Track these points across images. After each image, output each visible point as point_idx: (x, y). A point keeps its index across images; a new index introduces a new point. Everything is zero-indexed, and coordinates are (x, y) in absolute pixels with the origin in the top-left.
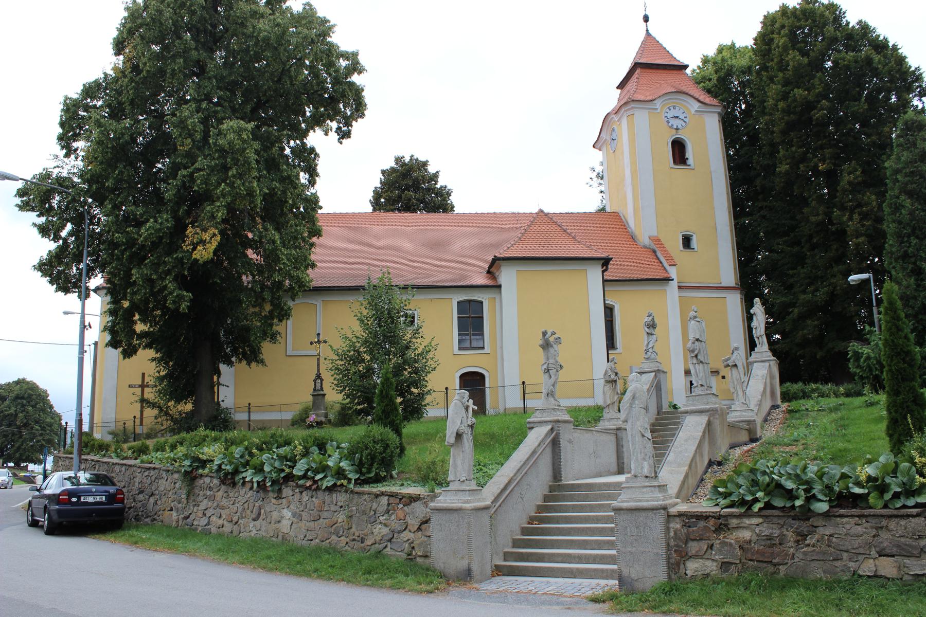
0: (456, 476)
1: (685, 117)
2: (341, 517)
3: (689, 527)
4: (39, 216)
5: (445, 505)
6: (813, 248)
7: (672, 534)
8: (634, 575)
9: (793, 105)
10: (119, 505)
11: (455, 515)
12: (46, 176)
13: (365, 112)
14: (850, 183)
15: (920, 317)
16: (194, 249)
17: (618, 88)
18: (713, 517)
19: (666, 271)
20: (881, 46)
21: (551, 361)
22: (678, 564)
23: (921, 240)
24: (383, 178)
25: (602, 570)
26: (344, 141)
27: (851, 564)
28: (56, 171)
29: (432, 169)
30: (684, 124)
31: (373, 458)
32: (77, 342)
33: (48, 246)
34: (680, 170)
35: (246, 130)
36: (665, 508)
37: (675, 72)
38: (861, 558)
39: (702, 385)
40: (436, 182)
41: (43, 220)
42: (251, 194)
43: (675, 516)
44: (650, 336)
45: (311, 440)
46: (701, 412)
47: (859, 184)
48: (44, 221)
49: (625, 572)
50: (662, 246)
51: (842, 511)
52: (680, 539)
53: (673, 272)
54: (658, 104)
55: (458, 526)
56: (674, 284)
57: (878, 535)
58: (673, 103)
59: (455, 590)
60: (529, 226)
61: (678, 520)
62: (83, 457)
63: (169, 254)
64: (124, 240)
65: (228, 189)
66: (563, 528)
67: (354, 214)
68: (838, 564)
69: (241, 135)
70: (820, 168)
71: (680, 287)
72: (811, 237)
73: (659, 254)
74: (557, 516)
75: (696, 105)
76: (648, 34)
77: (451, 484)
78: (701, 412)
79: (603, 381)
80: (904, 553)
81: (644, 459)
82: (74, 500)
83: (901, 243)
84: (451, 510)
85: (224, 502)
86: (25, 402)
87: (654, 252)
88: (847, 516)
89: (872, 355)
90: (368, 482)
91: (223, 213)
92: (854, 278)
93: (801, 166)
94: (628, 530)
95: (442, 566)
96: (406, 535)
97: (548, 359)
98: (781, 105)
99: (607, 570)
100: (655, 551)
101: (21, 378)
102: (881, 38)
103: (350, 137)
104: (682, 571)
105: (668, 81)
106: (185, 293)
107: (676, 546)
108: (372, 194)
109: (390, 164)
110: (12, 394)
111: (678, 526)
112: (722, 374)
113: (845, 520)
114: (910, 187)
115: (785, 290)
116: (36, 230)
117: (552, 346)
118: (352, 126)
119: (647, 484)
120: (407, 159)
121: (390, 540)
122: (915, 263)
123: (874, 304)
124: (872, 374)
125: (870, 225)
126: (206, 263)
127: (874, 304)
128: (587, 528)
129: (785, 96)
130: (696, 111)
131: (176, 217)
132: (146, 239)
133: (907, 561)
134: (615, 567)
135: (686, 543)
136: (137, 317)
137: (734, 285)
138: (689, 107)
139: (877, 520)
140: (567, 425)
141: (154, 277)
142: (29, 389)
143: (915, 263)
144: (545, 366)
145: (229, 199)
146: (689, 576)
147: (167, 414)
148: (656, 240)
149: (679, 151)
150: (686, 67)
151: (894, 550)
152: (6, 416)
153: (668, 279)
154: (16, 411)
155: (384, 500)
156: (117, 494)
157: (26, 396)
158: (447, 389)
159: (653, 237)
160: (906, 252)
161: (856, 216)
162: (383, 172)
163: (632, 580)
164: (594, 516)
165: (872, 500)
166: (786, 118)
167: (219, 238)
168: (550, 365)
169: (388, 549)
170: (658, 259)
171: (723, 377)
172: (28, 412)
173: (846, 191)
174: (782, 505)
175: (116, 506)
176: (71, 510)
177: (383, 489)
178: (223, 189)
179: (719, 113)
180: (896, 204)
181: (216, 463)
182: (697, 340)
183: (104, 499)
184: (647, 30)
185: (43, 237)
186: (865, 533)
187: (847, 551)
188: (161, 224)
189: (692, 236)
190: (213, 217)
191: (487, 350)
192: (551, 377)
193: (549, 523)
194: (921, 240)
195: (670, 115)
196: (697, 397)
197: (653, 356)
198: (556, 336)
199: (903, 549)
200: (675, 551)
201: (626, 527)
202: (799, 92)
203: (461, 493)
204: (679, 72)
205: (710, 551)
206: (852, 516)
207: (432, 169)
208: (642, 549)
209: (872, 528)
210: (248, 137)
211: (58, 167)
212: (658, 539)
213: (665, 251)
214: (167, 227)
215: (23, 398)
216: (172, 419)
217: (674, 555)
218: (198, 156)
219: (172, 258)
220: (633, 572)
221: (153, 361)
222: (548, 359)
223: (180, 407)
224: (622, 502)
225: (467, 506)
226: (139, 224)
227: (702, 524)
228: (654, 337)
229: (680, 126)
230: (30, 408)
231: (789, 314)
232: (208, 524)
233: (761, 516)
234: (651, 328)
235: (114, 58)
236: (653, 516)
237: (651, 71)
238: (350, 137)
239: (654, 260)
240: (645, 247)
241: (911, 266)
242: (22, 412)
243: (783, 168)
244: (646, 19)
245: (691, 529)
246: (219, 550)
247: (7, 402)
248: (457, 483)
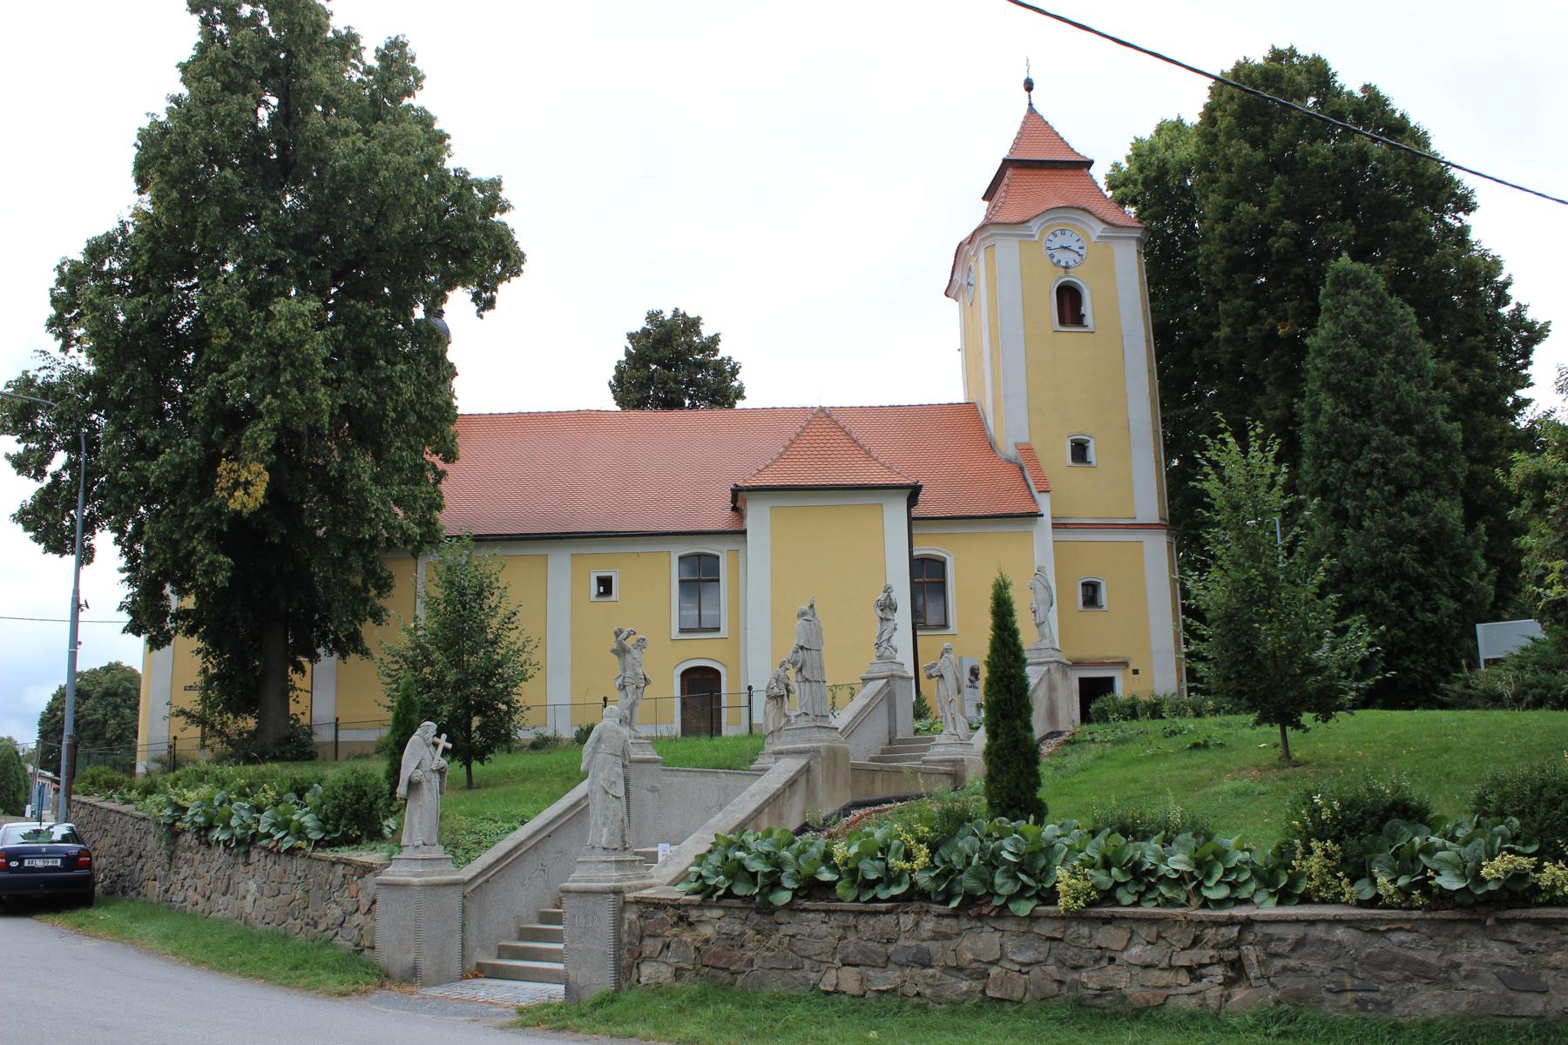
0: (410, 839)
1: (1081, 248)
2: (299, 893)
4: (19, 442)
5: (392, 878)
8: (581, 982)
9: (1238, 229)
10: (86, 872)
12: (26, 382)
13: (523, 267)
16: (231, 495)
17: (984, 198)
18: (671, 906)
19: (1034, 501)
20: (1398, 128)
21: (629, 673)
22: (630, 968)
24: (630, 347)
26: (485, 314)
27: (813, 976)
28: (44, 373)
29: (707, 331)
30: (1078, 259)
31: (342, 810)
32: (81, 625)
33: (27, 489)
34: (1071, 334)
35: (302, 314)
36: (617, 892)
37: (1071, 172)
38: (824, 967)
39: (806, 714)
40: (716, 352)
41: (20, 448)
42: (313, 405)
43: (631, 903)
44: (885, 623)
45: (288, 783)
46: (799, 752)
48: (21, 451)
49: (572, 975)
51: (808, 904)
53: (1045, 504)
54: (1035, 228)
57: (845, 938)
58: (1060, 224)
59: (393, 993)
60: (798, 435)
61: (635, 908)
62: (74, 797)
63: (198, 500)
64: (133, 480)
65: (276, 403)
67: (550, 414)
68: (797, 974)
69: (294, 324)
75: (1098, 229)
76: (1031, 109)
77: (404, 849)
78: (799, 752)
79: (764, 698)
80: (868, 962)
81: (604, 824)
82: (14, 864)
85: (201, 869)
86: (119, 700)
87: (1022, 469)
88: (813, 911)
90: (332, 844)
91: (269, 441)
96: (358, 919)
97: (625, 670)
98: (1220, 228)
101: (113, 661)
102: (1397, 115)
103: (493, 308)
104: (635, 977)
105: (1055, 190)
106: (221, 558)
107: (630, 943)
108: (614, 373)
109: (639, 323)
110: (98, 689)
111: (634, 917)
112: (1133, 666)
113: (811, 916)
114: (1334, 379)
116: (8, 464)
117: (629, 652)
118: (496, 290)
119: (604, 858)
120: (668, 315)
121: (341, 925)
126: (253, 514)
129: (1226, 215)
130: (1099, 237)
131: (208, 444)
132: (158, 479)
133: (871, 973)
134: (560, 966)
135: (641, 939)
136: (168, 589)
138: (1087, 229)
139: (844, 917)
140: (654, 766)
141: (176, 536)
142: (126, 679)
144: (619, 681)
145: (278, 419)
147: (221, 733)
149: (1069, 303)
150: (1089, 164)
151: (858, 959)
152: (90, 724)
153: (1035, 515)
154: (105, 715)
155: (340, 869)
156: (80, 854)
157: (120, 690)
158: (605, 699)
159: (1023, 444)
160: (1324, 482)
162: (631, 337)
165: (840, 889)
166: (1227, 251)
167: (267, 476)
169: (338, 937)
170: (1025, 480)
171: (1136, 672)
172: (123, 718)
174: (743, 894)
175: (76, 873)
176: (13, 879)
177: (339, 855)
178: (269, 404)
179: (1138, 239)
181: (189, 813)
182: (802, 648)
183: (59, 863)
184: (1030, 104)
185: (18, 473)
186: (830, 934)
187: (809, 958)
188: (184, 453)
189: (1088, 441)
190: (255, 447)
191: (724, 633)
195: (1056, 243)
197: (887, 653)
198: (639, 636)
199: (868, 957)
202: (1246, 209)
203: (413, 863)
204: (1077, 172)
205: (665, 951)
206: (817, 911)
207: (707, 331)
209: (838, 927)
210: (305, 324)
211: (45, 367)
213: (1037, 468)
214: (193, 460)
215: (115, 694)
216: (230, 742)
218: (242, 351)
219: (202, 507)
220: (580, 976)
221: (198, 653)
222: (625, 670)
223: (241, 724)
224: (573, 881)
225: (416, 880)
226: (154, 454)
227: (661, 914)
229: (1071, 263)
230: (127, 711)
232: (185, 900)
233: (723, 907)
234: (887, 610)
235: (137, 197)
237: (1029, 172)
238: (493, 308)
240: (1009, 461)
242: (114, 718)
244: (1029, 86)
245: (647, 922)
246: (167, 937)
247: (91, 702)
248: (411, 849)
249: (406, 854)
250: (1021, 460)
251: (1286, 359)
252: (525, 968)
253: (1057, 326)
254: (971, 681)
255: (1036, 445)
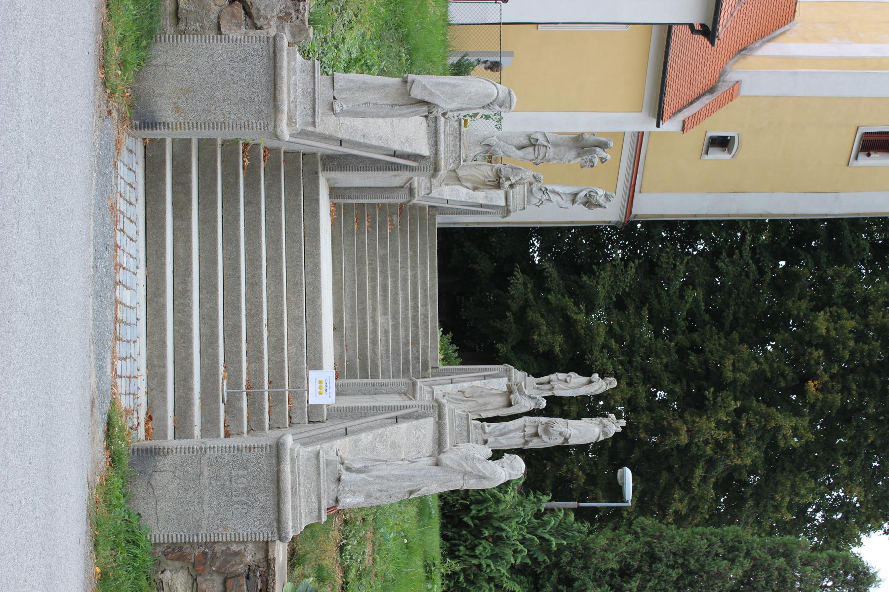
3: (248, 578)
5: (284, 73)
6: (682, 352)
7: (235, 548)
11: (264, 96)
14: (778, 428)
15: (555, 572)
19: (674, 114)
21: (551, 152)
23: (676, 584)
25: (163, 357)
34: (850, 141)
44: (570, 198)
47: (774, 438)
49: (165, 463)
50: (720, 104)
52: (226, 562)
53: (671, 126)
55: (242, 100)
56: (649, 126)
61: (260, 556)
66: (237, 228)
70: (810, 382)
71: (640, 136)
72: (699, 352)
73: (706, 100)
74: (259, 203)
81: (369, 496)
83: (674, 554)
84: (275, 89)
87: (711, 90)
89: (502, 507)
92: (627, 476)
93: (821, 352)
94: (241, 472)
95: (159, 61)
97: (555, 145)
99: (164, 366)
100: (205, 522)
107: (214, 555)
111: (249, 558)
114: (762, 575)
115: (617, 296)
122: (639, 570)
123: (582, 504)
124: (472, 503)
125: (705, 452)
127: (582, 504)
128: (239, 278)
135: (219, 572)
137: (634, 212)
143: (639, 570)
144: (542, 141)
146: (161, 576)
148: (733, 93)
153: (660, 117)
159: (739, 90)
160: (660, 560)
161: (722, 435)
163: (151, 476)
164: (260, 278)
168: (543, 150)
170: (698, 98)
173: (766, 421)
180: (738, 550)
189: (730, 152)
192: (521, 148)
193: (246, 186)
194: (676, 584)
196: (465, 433)
197: (535, 201)
200: (205, 554)
201: (246, 468)
203: (308, 105)
208: (206, 498)
212: (226, 528)
217: (197, 552)
222: (555, 145)
228: (569, 204)
231: (576, 304)
236: (268, 522)
239: (698, 91)
240: (723, 73)
241: (636, 564)
243: (822, 323)
245: (243, 581)
248: (329, 93)
249: (322, 81)
250: (722, 89)
251: (783, 384)
252: (163, 227)
253: (862, 130)
254: (486, 62)
255: (736, 101)
